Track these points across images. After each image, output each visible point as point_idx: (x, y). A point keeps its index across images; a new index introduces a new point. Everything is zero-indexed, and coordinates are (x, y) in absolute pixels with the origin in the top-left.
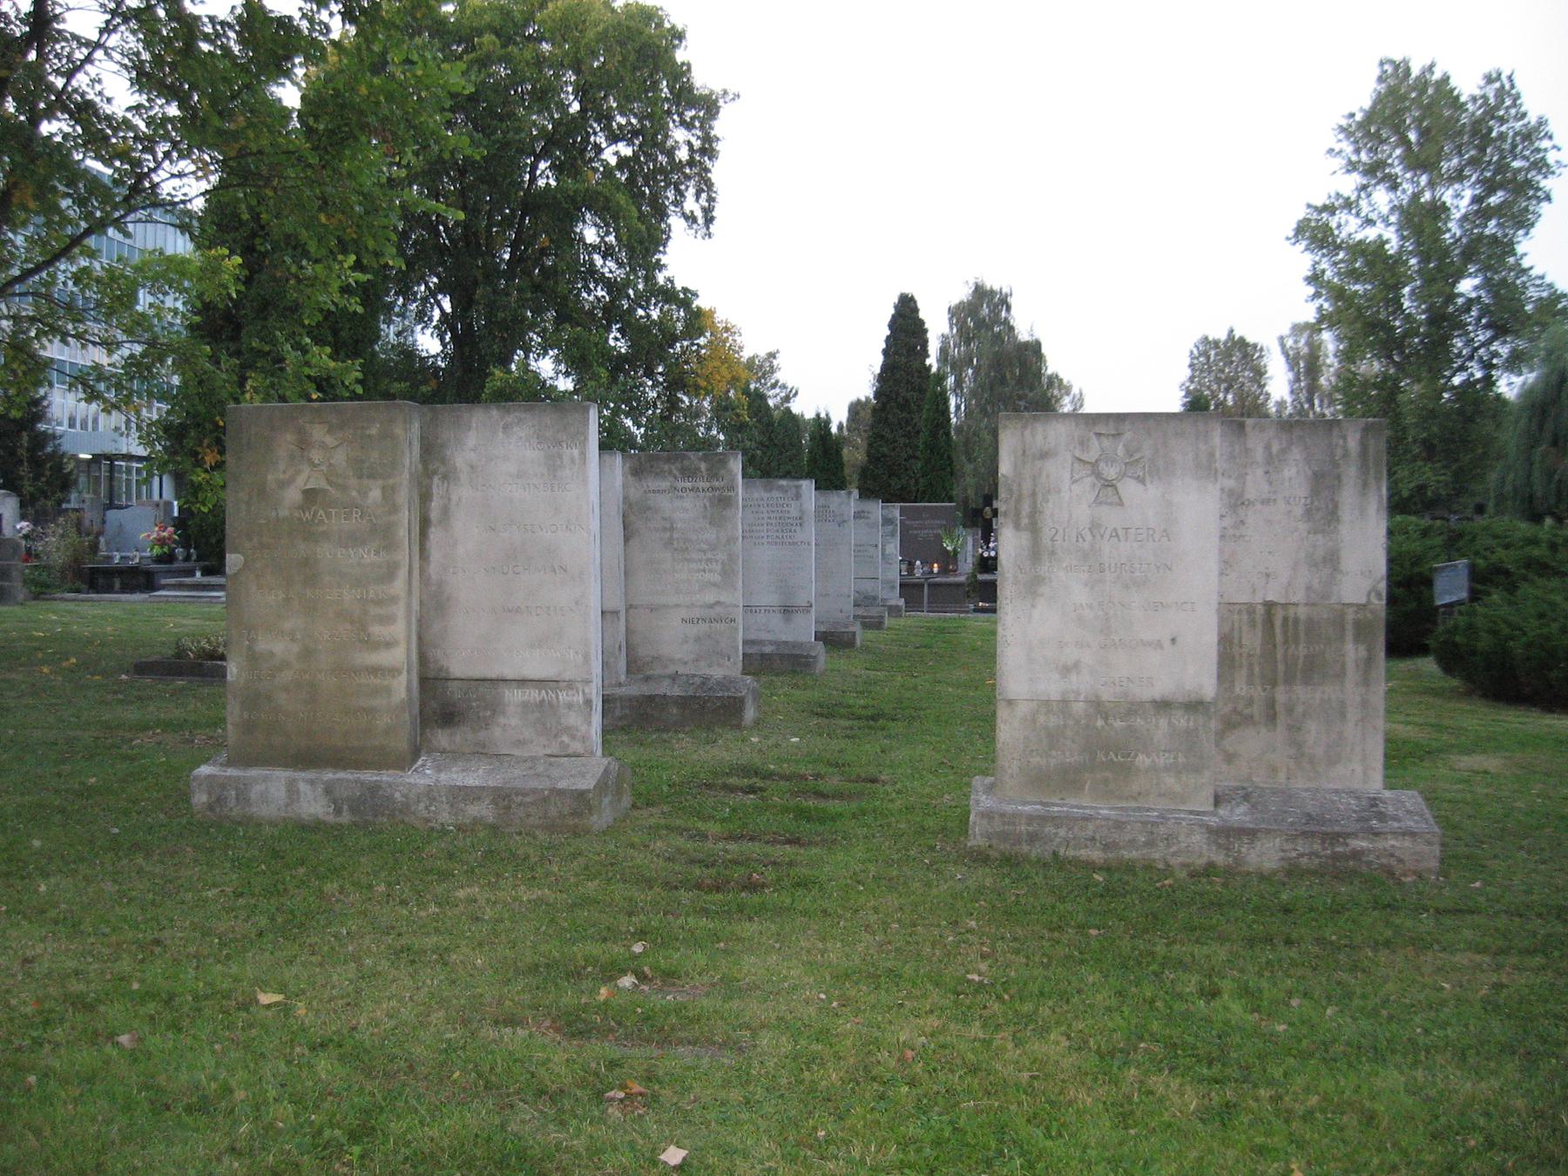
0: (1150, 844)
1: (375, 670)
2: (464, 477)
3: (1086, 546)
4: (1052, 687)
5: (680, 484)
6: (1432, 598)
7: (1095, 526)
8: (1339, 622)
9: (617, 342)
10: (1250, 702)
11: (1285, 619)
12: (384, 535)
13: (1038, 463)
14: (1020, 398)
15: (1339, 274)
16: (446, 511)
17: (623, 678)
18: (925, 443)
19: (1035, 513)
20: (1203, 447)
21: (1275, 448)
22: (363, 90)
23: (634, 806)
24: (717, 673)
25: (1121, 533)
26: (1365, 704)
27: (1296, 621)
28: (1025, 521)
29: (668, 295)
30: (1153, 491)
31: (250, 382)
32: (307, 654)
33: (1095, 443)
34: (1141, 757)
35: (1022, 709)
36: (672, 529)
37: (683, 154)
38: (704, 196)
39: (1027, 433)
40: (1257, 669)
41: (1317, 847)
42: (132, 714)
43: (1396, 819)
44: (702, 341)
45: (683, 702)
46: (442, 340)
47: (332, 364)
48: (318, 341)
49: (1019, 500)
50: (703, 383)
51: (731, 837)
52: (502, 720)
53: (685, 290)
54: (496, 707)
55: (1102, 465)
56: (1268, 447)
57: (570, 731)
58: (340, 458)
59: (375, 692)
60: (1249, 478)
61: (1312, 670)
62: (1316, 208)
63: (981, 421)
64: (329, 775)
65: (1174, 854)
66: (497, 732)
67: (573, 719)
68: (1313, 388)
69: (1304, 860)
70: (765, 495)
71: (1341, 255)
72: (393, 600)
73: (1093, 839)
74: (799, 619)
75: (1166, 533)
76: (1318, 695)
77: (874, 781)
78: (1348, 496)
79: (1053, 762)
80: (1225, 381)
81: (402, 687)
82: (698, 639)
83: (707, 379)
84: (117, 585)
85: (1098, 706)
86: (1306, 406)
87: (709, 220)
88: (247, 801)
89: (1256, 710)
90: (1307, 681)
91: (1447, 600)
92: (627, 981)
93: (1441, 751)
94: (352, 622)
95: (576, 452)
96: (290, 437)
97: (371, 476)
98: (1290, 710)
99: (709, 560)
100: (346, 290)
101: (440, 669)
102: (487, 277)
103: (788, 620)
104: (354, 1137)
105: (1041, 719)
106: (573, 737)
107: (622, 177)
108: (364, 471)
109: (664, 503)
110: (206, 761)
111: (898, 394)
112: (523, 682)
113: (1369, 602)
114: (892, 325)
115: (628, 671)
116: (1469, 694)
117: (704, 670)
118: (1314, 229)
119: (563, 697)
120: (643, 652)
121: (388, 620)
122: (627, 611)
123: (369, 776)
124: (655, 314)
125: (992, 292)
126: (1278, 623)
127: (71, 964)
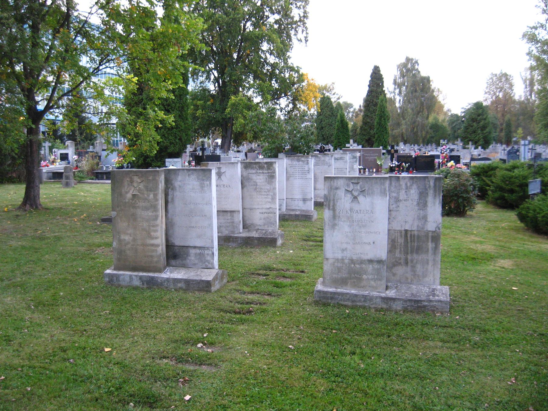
0: (364, 301)
1: (153, 245)
2: (177, 189)
3: (349, 215)
4: (339, 256)
5: (259, 171)
6: (527, 192)
7: (351, 210)
8: (427, 236)
9: (275, 85)
10: (400, 259)
11: (411, 235)
12: (154, 208)
13: (335, 191)
14: (422, 97)
15: (538, 52)
16: (173, 199)
17: (241, 231)
18: (377, 123)
19: (334, 205)
20: (383, 187)
21: (409, 184)
22: (170, 31)
23: (228, 282)
24: (270, 229)
25: (359, 211)
26: (434, 260)
27: (414, 235)
28: (331, 207)
29: (292, 69)
30: (368, 199)
31: (138, 124)
32: (134, 240)
33: (351, 185)
34: (364, 276)
35: (331, 261)
36: (256, 185)
37: (297, 18)
38: (305, 32)
39: (332, 182)
40: (402, 249)
41: (413, 304)
42: (97, 239)
43: (438, 296)
44: (304, 84)
45: (259, 239)
46: (215, 86)
47: (165, 116)
48: (161, 110)
49: (330, 201)
50: (304, 99)
51: (252, 293)
52: (189, 258)
53: (298, 67)
54: (188, 255)
55: (353, 192)
56: (406, 184)
57: (207, 261)
58: (141, 186)
59: (153, 251)
60: (400, 193)
61: (418, 250)
62: (530, 27)
63: (408, 105)
64: (141, 274)
65: (372, 304)
66: (188, 261)
67: (208, 258)
68: (531, 91)
69: (409, 308)
70: (297, 163)
71: (539, 44)
72: (157, 225)
73: (349, 299)
74: (308, 203)
75: (372, 212)
76: (420, 257)
77: (303, 272)
78: (430, 199)
79: (339, 276)
80: (499, 88)
81: (162, 249)
82: (264, 219)
83: (305, 98)
84: (105, 177)
85: (352, 261)
86: (529, 97)
87: (306, 41)
88: (119, 281)
89: (402, 261)
90: (417, 253)
91: (533, 193)
92: (200, 345)
93: (496, 257)
94: (146, 231)
95: (208, 183)
96: (128, 179)
97: (151, 191)
98: (412, 261)
99: (267, 195)
100: (168, 91)
101: (172, 243)
102: (229, 65)
103: (304, 203)
104: (117, 389)
105: (336, 264)
106: (209, 263)
107: (276, 26)
108: (148, 189)
109: (254, 177)
110: (108, 268)
111: (373, 101)
112: (195, 247)
113: (436, 230)
114: (371, 76)
115: (243, 228)
116: (528, 230)
117: (266, 227)
118: (529, 35)
119: (206, 252)
120: (248, 222)
121: (156, 231)
122: (243, 210)
123: (151, 274)
124: (287, 75)
125: (412, 59)
126: (409, 236)
127: (63, 337)
